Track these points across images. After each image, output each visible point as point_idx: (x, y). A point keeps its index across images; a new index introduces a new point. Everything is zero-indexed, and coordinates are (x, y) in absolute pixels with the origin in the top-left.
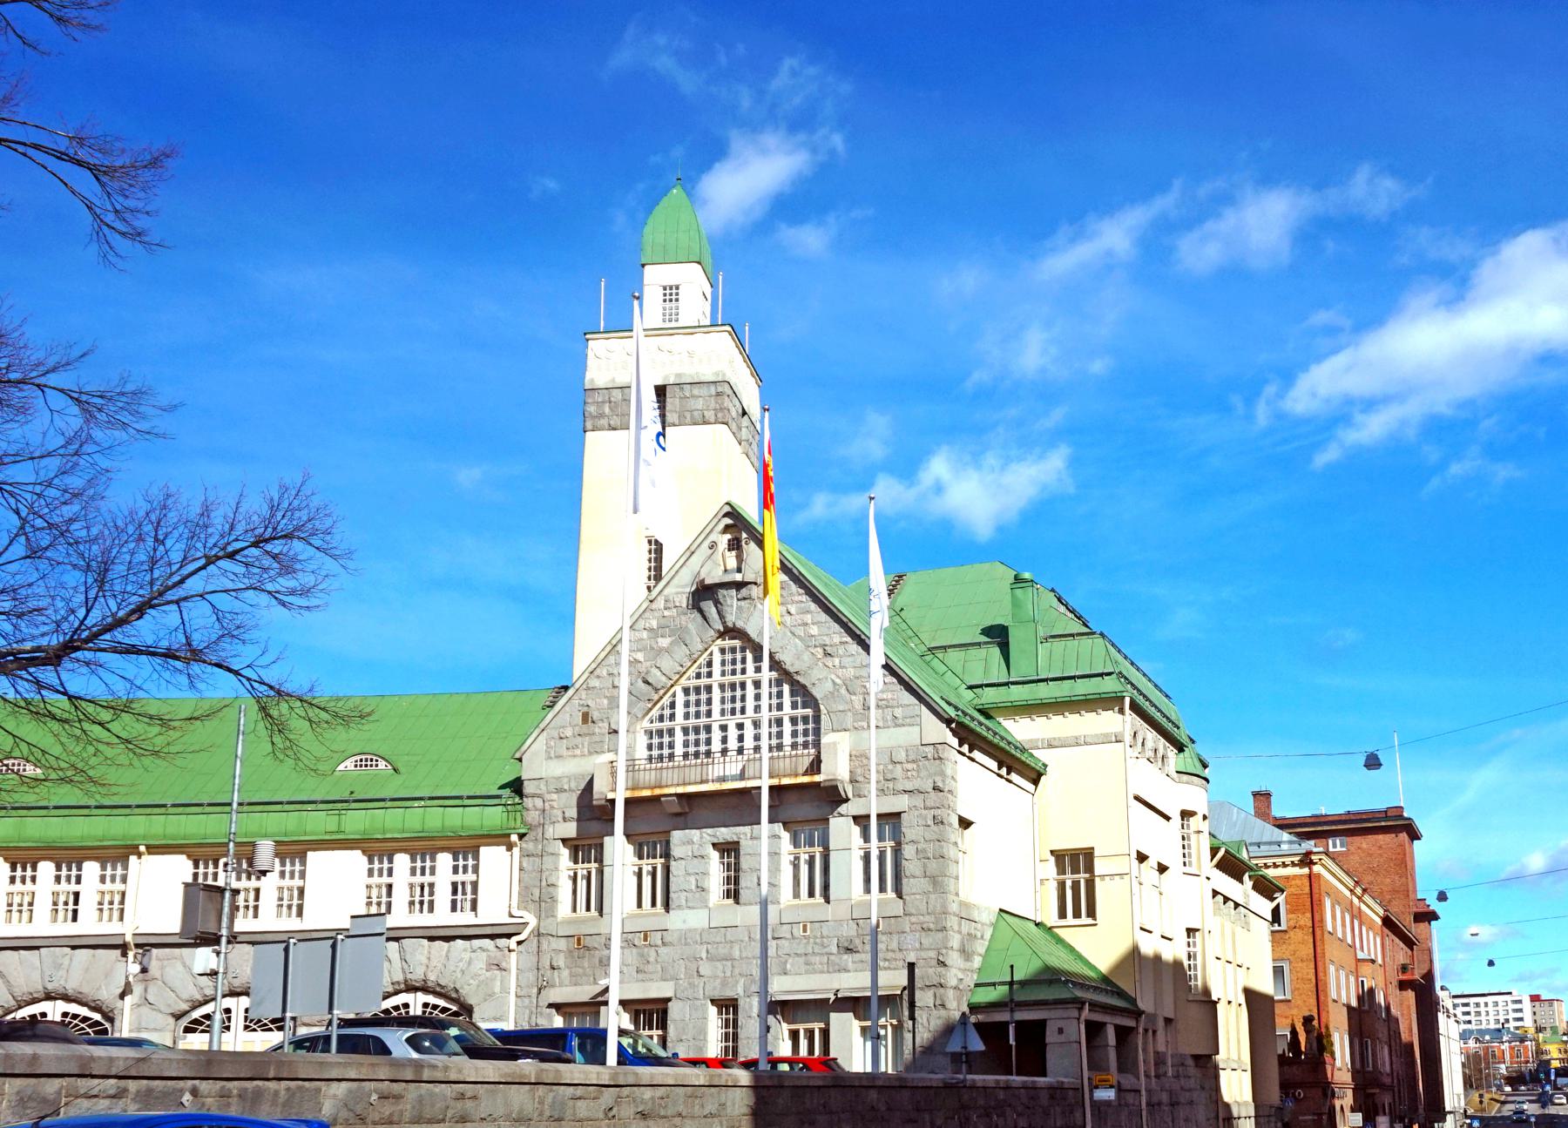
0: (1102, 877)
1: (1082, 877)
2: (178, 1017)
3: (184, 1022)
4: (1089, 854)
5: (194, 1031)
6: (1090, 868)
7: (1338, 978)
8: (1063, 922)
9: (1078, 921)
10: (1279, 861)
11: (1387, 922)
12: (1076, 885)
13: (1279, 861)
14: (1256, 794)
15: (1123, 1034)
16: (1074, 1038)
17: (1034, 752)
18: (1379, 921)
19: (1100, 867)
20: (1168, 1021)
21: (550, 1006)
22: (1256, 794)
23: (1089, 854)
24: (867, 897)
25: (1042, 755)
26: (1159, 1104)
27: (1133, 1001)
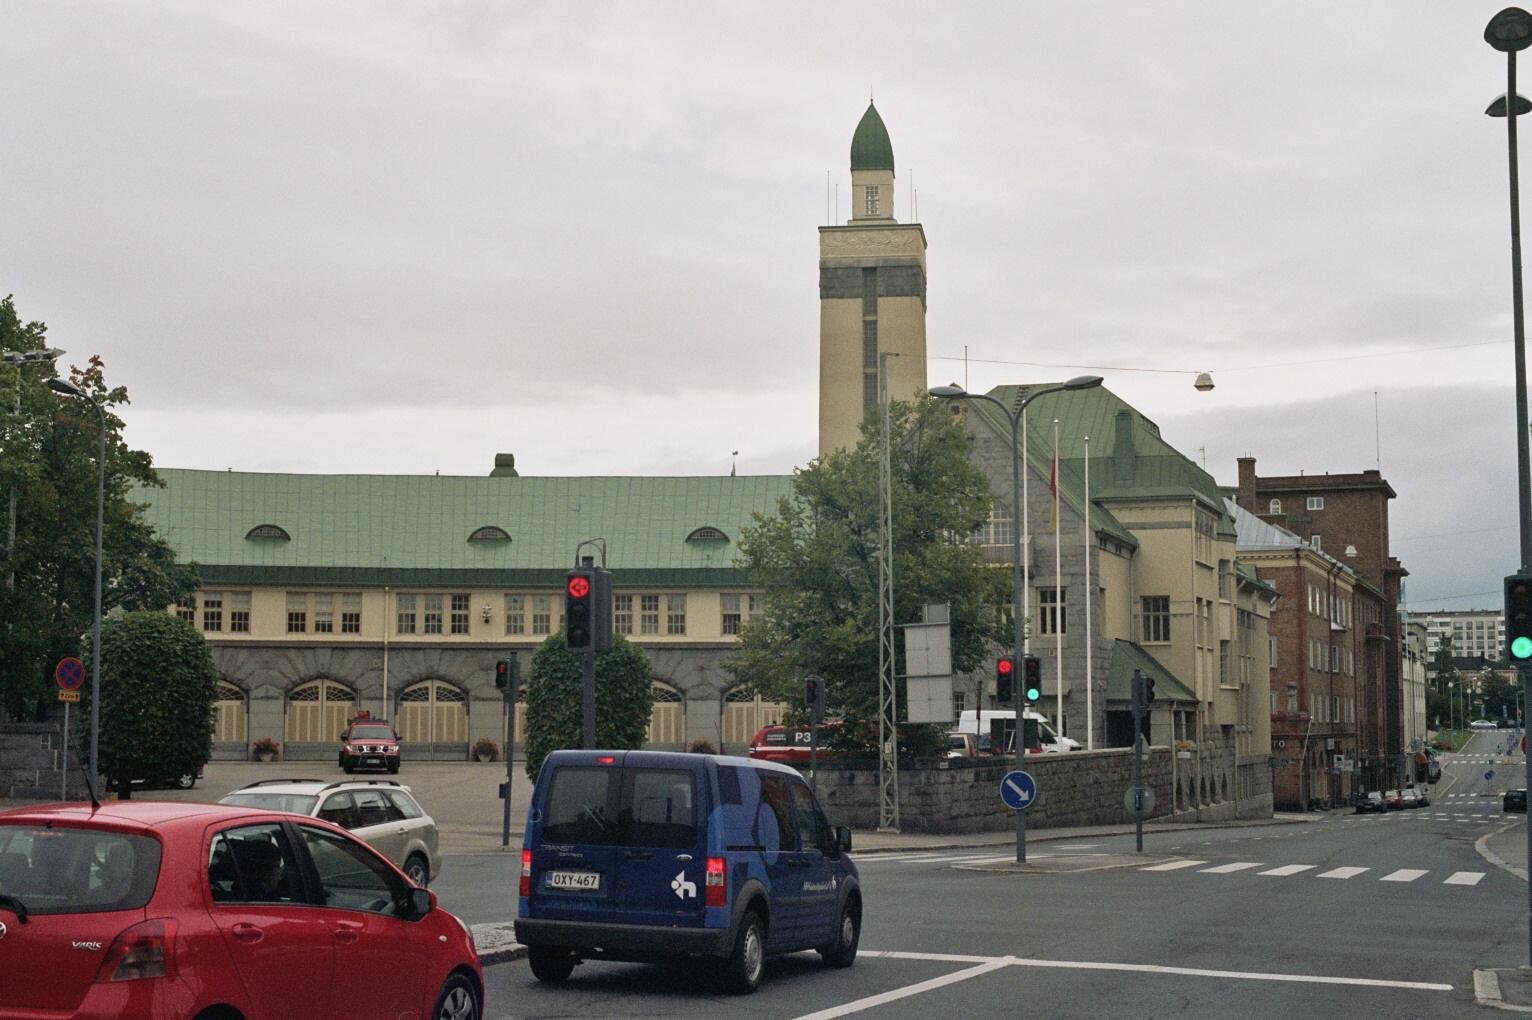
0: (1175, 615)
1: (1161, 614)
2: (723, 691)
3: (726, 695)
4: (1166, 600)
5: (732, 700)
6: (1166, 608)
7: (1315, 650)
8: (1148, 643)
9: (1156, 643)
10: (1271, 555)
11: (1359, 588)
12: (1157, 619)
13: (1271, 555)
14: (1240, 461)
15: (1189, 715)
16: (1168, 722)
17: (1131, 531)
18: (1350, 589)
19: (1173, 609)
20: (1210, 704)
21: (150, 505)
22: (1240, 461)
23: (1166, 600)
24: (1053, 635)
25: (1138, 534)
26: (1205, 758)
27: (1193, 694)
